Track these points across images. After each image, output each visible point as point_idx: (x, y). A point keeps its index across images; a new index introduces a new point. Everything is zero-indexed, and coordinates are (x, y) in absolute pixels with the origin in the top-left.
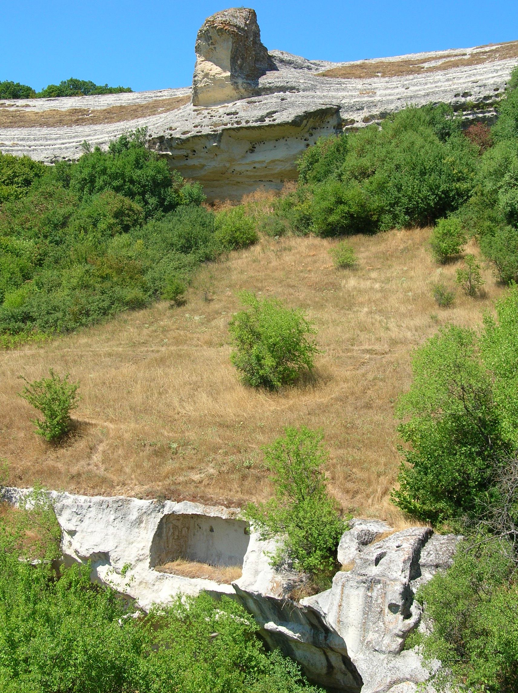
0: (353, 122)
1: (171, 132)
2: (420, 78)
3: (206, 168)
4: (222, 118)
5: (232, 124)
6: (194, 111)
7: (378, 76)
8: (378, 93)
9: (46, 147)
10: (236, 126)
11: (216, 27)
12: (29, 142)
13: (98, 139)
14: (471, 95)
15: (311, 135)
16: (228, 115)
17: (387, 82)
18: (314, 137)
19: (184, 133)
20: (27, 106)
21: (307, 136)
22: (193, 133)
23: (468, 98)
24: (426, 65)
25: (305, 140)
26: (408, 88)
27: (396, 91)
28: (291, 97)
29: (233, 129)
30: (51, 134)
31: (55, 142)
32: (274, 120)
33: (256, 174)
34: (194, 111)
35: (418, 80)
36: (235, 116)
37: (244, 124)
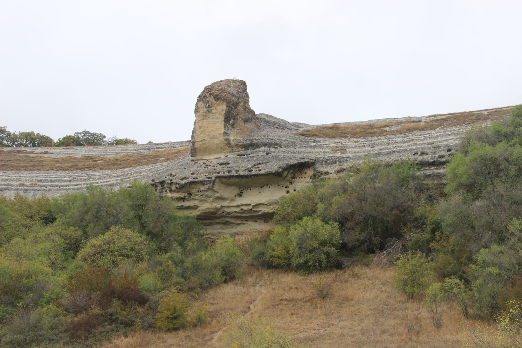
0: (327, 173)
1: (171, 178)
2: (384, 139)
3: (199, 208)
4: (215, 168)
5: (224, 173)
6: (192, 161)
8: (348, 150)
9: (61, 188)
11: (213, 93)
12: (46, 183)
14: (427, 154)
15: (291, 183)
16: (221, 165)
18: (293, 185)
20: (46, 153)
21: (288, 184)
22: (191, 179)
23: (425, 157)
24: (388, 129)
25: (286, 187)
28: (274, 152)
29: (225, 177)
30: (65, 177)
32: (260, 170)
34: (192, 161)
36: (226, 166)
37: (234, 173)
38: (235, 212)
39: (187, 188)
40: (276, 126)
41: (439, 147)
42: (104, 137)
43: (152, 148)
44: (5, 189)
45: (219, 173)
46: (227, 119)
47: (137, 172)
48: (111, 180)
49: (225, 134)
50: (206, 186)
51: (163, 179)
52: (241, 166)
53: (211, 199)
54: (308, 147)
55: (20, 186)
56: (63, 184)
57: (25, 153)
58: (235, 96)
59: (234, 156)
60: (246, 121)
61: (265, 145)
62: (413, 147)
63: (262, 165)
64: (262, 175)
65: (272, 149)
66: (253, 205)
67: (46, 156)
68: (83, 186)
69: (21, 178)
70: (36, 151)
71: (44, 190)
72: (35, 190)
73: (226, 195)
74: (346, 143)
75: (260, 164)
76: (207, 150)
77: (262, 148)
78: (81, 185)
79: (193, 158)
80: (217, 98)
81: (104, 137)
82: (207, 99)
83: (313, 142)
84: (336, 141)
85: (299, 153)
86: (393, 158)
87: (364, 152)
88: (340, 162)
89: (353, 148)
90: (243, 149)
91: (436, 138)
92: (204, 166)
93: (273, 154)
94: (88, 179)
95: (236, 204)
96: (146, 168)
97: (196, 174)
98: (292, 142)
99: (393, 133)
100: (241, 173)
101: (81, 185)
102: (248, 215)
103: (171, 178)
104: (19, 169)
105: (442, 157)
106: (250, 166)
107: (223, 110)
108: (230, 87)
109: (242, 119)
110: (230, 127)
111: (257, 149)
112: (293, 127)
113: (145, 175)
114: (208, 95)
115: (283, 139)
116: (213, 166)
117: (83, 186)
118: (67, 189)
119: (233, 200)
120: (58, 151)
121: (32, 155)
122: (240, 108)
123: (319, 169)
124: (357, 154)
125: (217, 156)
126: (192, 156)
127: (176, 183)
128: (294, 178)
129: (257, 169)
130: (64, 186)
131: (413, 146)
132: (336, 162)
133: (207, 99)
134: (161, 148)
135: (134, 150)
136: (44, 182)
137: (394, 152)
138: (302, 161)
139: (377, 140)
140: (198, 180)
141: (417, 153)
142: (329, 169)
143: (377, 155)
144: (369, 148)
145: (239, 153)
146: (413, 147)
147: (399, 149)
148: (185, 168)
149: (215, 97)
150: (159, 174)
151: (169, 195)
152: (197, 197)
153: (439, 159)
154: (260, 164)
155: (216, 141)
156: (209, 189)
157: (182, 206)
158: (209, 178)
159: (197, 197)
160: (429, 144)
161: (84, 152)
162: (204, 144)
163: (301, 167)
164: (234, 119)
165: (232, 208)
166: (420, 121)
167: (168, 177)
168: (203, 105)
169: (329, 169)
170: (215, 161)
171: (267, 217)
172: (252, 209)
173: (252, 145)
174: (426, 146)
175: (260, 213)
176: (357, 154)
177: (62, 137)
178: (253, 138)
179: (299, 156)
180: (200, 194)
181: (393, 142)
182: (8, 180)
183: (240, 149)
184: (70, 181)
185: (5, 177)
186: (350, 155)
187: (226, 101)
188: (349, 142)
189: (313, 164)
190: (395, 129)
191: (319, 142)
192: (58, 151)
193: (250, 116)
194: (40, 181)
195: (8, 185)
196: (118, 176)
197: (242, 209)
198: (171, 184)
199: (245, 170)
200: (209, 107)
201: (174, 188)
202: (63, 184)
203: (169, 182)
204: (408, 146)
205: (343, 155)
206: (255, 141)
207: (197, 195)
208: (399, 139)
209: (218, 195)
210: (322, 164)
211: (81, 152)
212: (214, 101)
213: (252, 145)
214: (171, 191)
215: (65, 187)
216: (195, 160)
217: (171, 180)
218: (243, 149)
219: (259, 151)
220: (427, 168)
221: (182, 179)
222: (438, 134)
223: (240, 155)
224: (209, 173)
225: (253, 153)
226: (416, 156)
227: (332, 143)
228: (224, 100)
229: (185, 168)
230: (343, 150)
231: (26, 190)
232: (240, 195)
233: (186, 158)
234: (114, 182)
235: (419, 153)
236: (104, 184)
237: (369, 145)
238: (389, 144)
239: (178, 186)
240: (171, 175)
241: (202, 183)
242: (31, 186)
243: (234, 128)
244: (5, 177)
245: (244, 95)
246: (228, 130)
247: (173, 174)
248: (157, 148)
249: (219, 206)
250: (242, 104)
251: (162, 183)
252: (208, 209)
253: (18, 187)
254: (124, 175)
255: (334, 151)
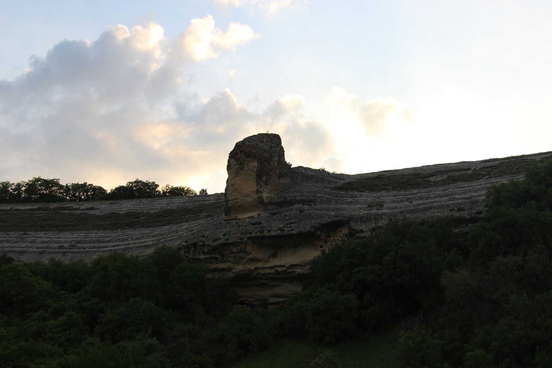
0: (362, 231)
1: (203, 239)
2: (423, 192)
3: (234, 271)
4: (247, 228)
5: (256, 233)
6: (225, 220)
7: (389, 189)
8: (385, 206)
9: (99, 249)
10: (259, 234)
12: (85, 245)
13: (143, 242)
14: (464, 210)
16: (253, 224)
17: (394, 196)
19: (215, 240)
20: (93, 209)
21: (322, 243)
22: (223, 241)
23: (462, 213)
24: (432, 179)
25: (321, 247)
26: (412, 202)
27: (401, 204)
28: (308, 210)
30: (105, 237)
31: (107, 244)
32: (292, 230)
33: (278, 277)
34: (225, 220)
35: (422, 194)
37: (266, 233)
38: (270, 273)
39: (220, 250)
40: (314, 179)
41: (477, 202)
42: (157, 186)
43: (198, 201)
44: (44, 252)
45: (251, 233)
46: (259, 176)
47: (174, 231)
48: (148, 240)
49: (258, 191)
50: (239, 248)
51: (196, 240)
52: (275, 227)
53: (244, 261)
54: (343, 203)
55: (58, 248)
56: (102, 245)
57: (71, 210)
58: (267, 152)
59: (267, 215)
60: (281, 176)
61: (299, 202)
62: (451, 202)
63: (295, 224)
64: (294, 235)
65: (306, 207)
66: (287, 266)
67: (91, 212)
68: (120, 247)
69: (61, 239)
70: (81, 208)
71: (81, 252)
72: (74, 252)
73: (259, 256)
74: (385, 198)
75: (292, 223)
76: (242, 208)
77: (297, 206)
78: (118, 245)
79: (226, 218)
80: (248, 155)
81: (157, 186)
82: (239, 156)
83: (350, 197)
84: (374, 195)
85: (334, 210)
86: (428, 214)
87: (401, 208)
88: (375, 219)
89: (390, 203)
90: (277, 207)
91: (476, 191)
92: (236, 226)
93: (306, 212)
94: (127, 239)
95: (270, 265)
96: (185, 226)
97: (228, 235)
98: (327, 198)
99: (436, 184)
100: (273, 233)
101: (118, 245)
102: (283, 276)
103: (203, 239)
104: (60, 228)
105: (480, 213)
106: (282, 226)
107: (255, 167)
108: (262, 142)
109: (277, 175)
110: (263, 184)
111: (291, 207)
112: (332, 179)
113: (175, 236)
114: (239, 152)
115: (318, 195)
116: (246, 226)
117: (120, 247)
118: (104, 251)
119: (267, 261)
120: (103, 206)
121: (78, 212)
122: (274, 163)
123: (353, 227)
124: (392, 211)
125: (250, 215)
126: (226, 215)
127: (208, 245)
128: (329, 237)
129: (289, 229)
130: (102, 247)
131: (451, 201)
132: (371, 219)
133: (239, 156)
134: (207, 200)
135: (180, 203)
136: (83, 244)
137: (431, 208)
138: (336, 219)
139: (416, 194)
140: (230, 241)
141: (453, 210)
142: (364, 227)
143: (412, 211)
144: (407, 203)
145: (272, 211)
146: (451, 202)
147: (436, 204)
148: (217, 229)
149: (245, 154)
150: (193, 234)
151: (202, 257)
152: (230, 259)
153: (476, 216)
154: (292, 223)
155: (249, 199)
156: (241, 251)
157: (216, 268)
158: (241, 239)
159: (230, 259)
160: (467, 198)
161: (129, 207)
162: (237, 202)
163: (334, 226)
164: (267, 176)
165: (266, 270)
166: (469, 169)
167: (200, 239)
168: (235, 163)
169: (364, 227)
170: (247, 220)
171: (300, 278)
172: (286, 270)
173: (286, 203)
174: (464, 201)
175: (295, 275)
176: (392, 211)
177: (114, 188)
178: (287, 195)
179: (333, 214)
180: (233, 255)
181: (432, 196)
182: (47, 242)
183: (274, 207)
184: (108, 242)
185: (45, 239)
186: (386, 211)
187: (258, 156)
188: (386, 197)
189: (348, 222)
190: (439, 179)
191: (356, 197)
192: (103, 206)
193: (286, 171)
194: (79, 242)
195: (48, 247)
196: (156, 236)
197: (277, 271)
198: (204, 246)
199: (277, 230)
200: (241, 164)
201: (206, 250)
202: (102, 245)
203: (201, 243)
204: (446, 201)
205: (379, 212)
206: (289, 198)
207: (231, 257)
208: (438, 192)
209: (251, 256)
210: (357, 222)
211: (126, 207)
212: (245, 158)
213: (286, 203)
214: (204, 253)
215: (103, 249)
216: (229, 220)
217: (203, 242)
218: (277, 207)
219: (292, 209)
220: (464, 225)
221: (215, 240)
222: (479, 187)
223: (273, 214)
224: (242, 234)
225: (286, 211)
226: (452, 212)
227: (367, 197)
228: (255, 157)
229: (217, 229)
230: (380, 205)
231: (64, 253)
232: (275, 256)
233: (221, 217)
234: (151, 243)
235: (456, 209)
236: (141, 244)
237: (407, 200)
238: (427, 198)
239: (209, 248)
240: (204, 236)
241: (234, 244)
242: (70, 249)
243: (267, 185)
244: (45, 239)
245: (278, 149)
246: (261, 187)
247: (206, 235)
248: (203, 201)
249: (253, 268)
250: (276, 159)
251: (195, 245)
252: (242, 271)
253: (57, 250)
254: (161, 235)
255: (370, 206)
